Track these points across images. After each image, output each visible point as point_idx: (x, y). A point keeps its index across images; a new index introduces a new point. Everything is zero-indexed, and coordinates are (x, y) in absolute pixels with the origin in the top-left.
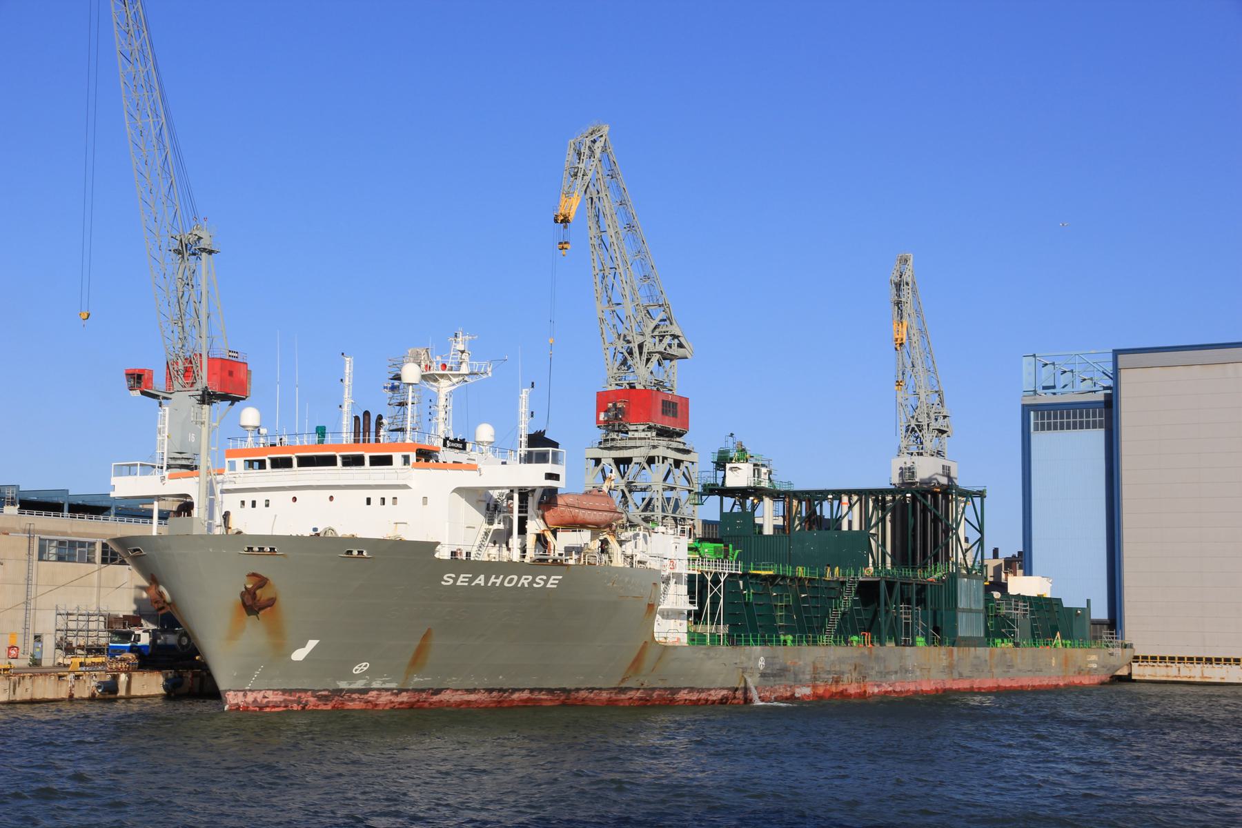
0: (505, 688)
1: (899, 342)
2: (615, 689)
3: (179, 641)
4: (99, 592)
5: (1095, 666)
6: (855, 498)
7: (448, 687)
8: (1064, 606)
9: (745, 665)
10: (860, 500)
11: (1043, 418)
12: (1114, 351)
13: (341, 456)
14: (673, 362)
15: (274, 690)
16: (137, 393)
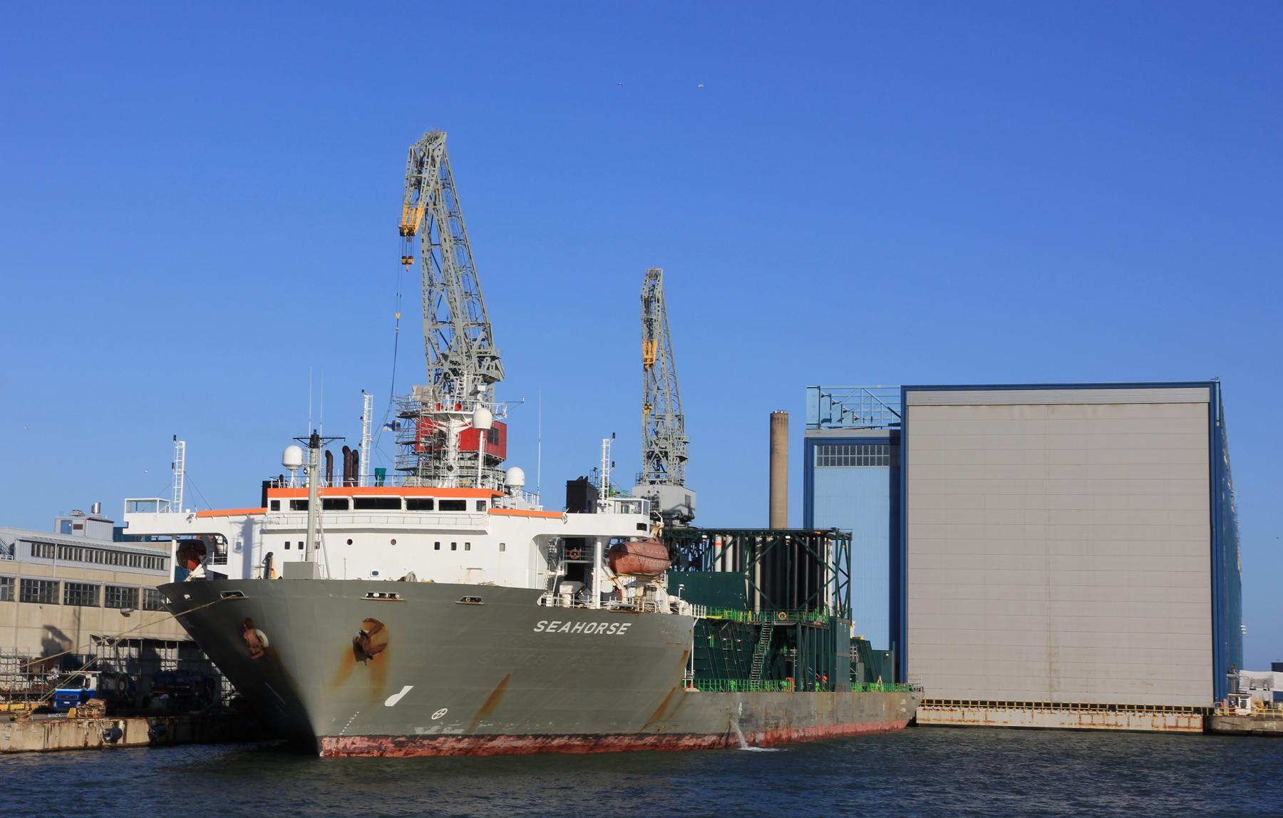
0: (550, 734)
1: (648, 362)
2: (636, 734)
3: (118, 686)
4: (17, 632)
5: (904, 710)
6: (729, 539)
7: (502, 733)
8: (873, 649)
10: (734, 543)
11: (827, 453)
12: (903, 387)
13: (405, 499)
14: (492, 386)
15: (362, 736)
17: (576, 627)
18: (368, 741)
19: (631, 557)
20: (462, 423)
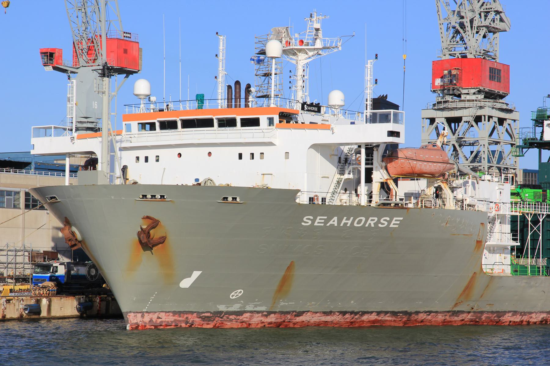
2: (449, 312)
3: (89, 272)
15: (166, 312)
16: (50, 68)
17: (344, 221)
18: (173, 316)
19: (400, 161)
20: (307, 56)
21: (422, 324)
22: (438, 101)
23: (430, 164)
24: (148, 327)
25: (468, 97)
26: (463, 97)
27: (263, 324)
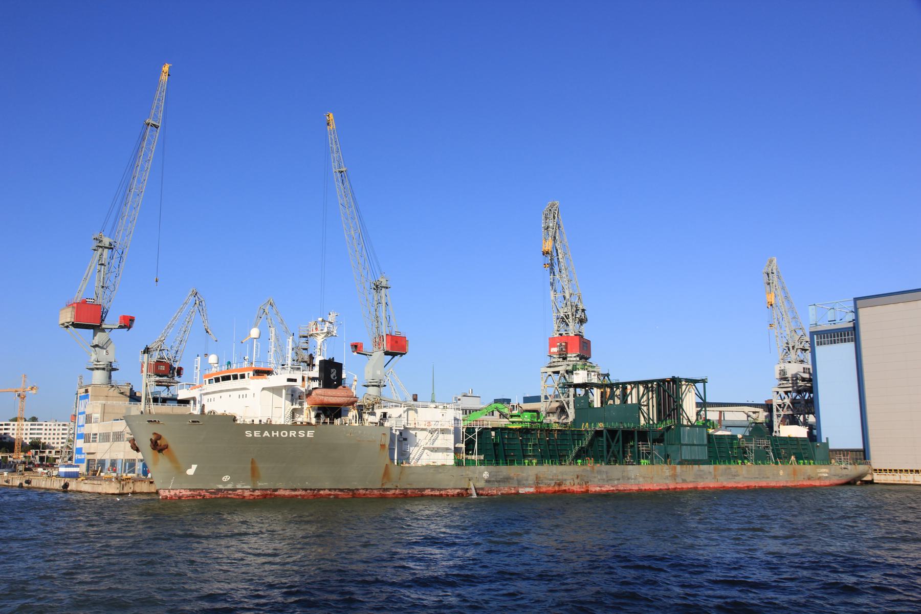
9: (470, 476)
12: (854, 298)
15: (185, 489)
16: (355, 353)
21: (364, 496)
22: (780, 369)
23: (336, 398)
24: (174, 498)
25: (572, 359)
26: (568, 359)
27: (253, 497)
